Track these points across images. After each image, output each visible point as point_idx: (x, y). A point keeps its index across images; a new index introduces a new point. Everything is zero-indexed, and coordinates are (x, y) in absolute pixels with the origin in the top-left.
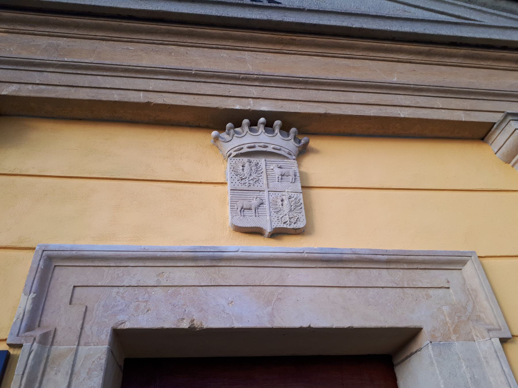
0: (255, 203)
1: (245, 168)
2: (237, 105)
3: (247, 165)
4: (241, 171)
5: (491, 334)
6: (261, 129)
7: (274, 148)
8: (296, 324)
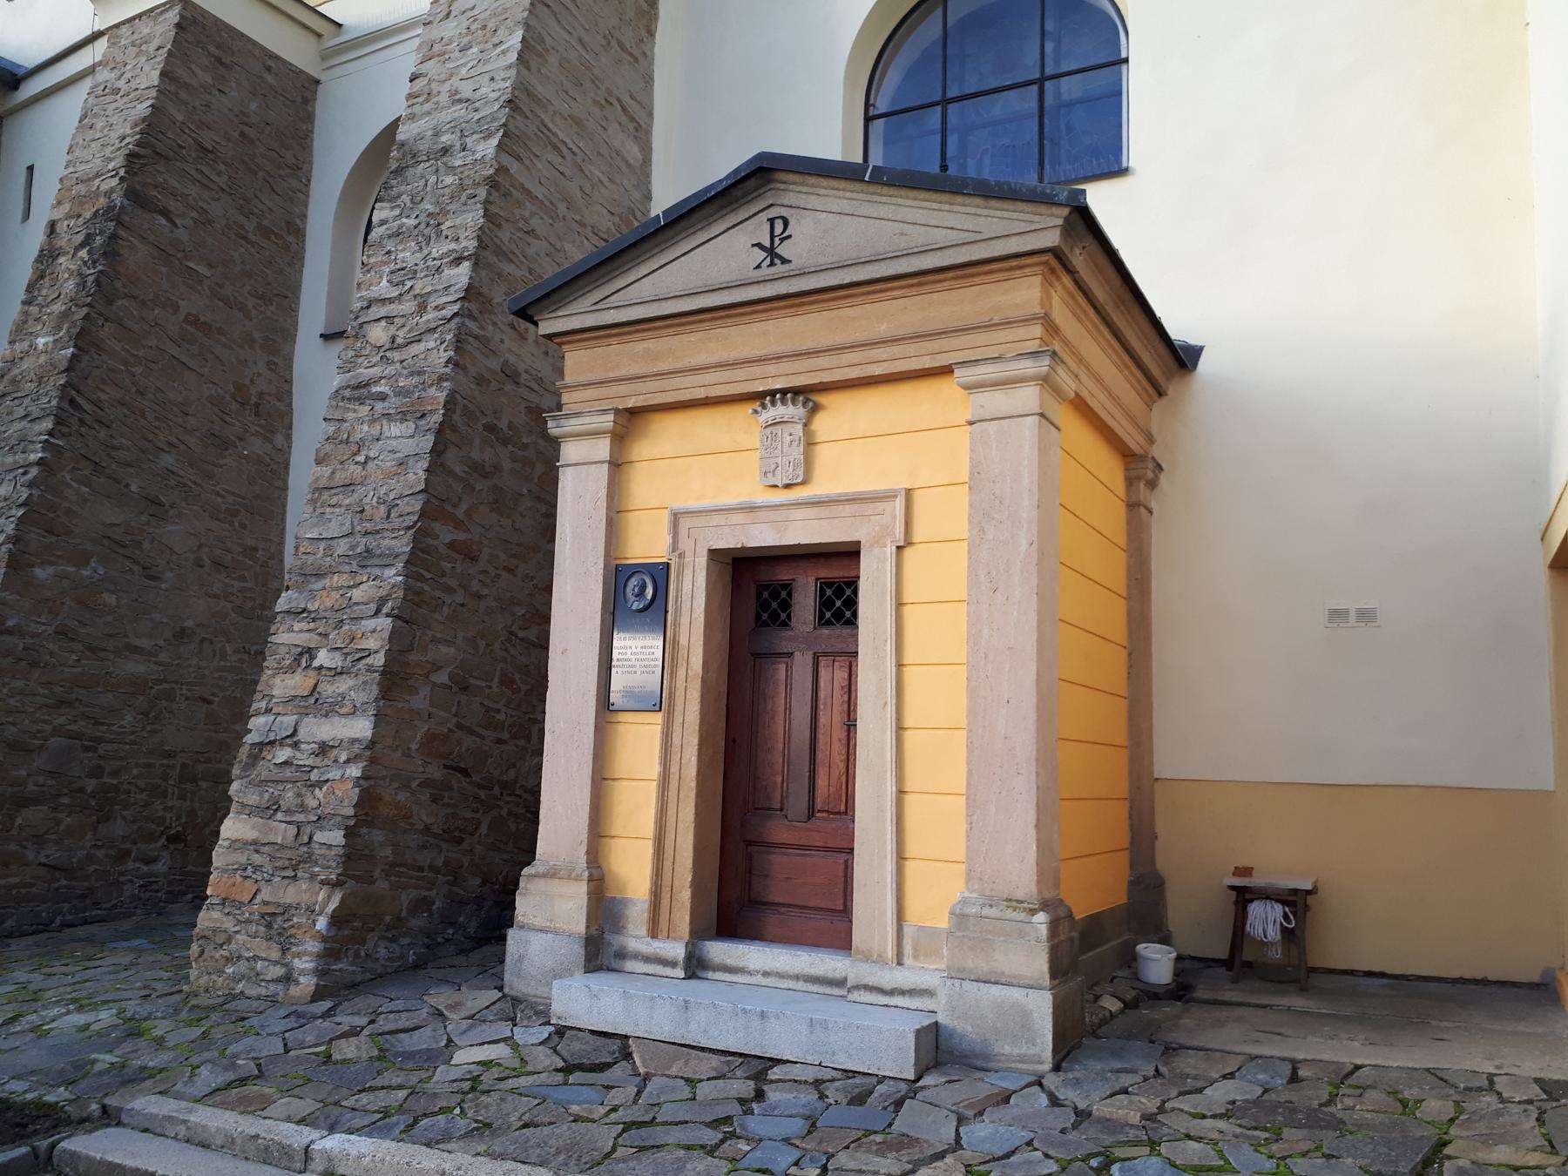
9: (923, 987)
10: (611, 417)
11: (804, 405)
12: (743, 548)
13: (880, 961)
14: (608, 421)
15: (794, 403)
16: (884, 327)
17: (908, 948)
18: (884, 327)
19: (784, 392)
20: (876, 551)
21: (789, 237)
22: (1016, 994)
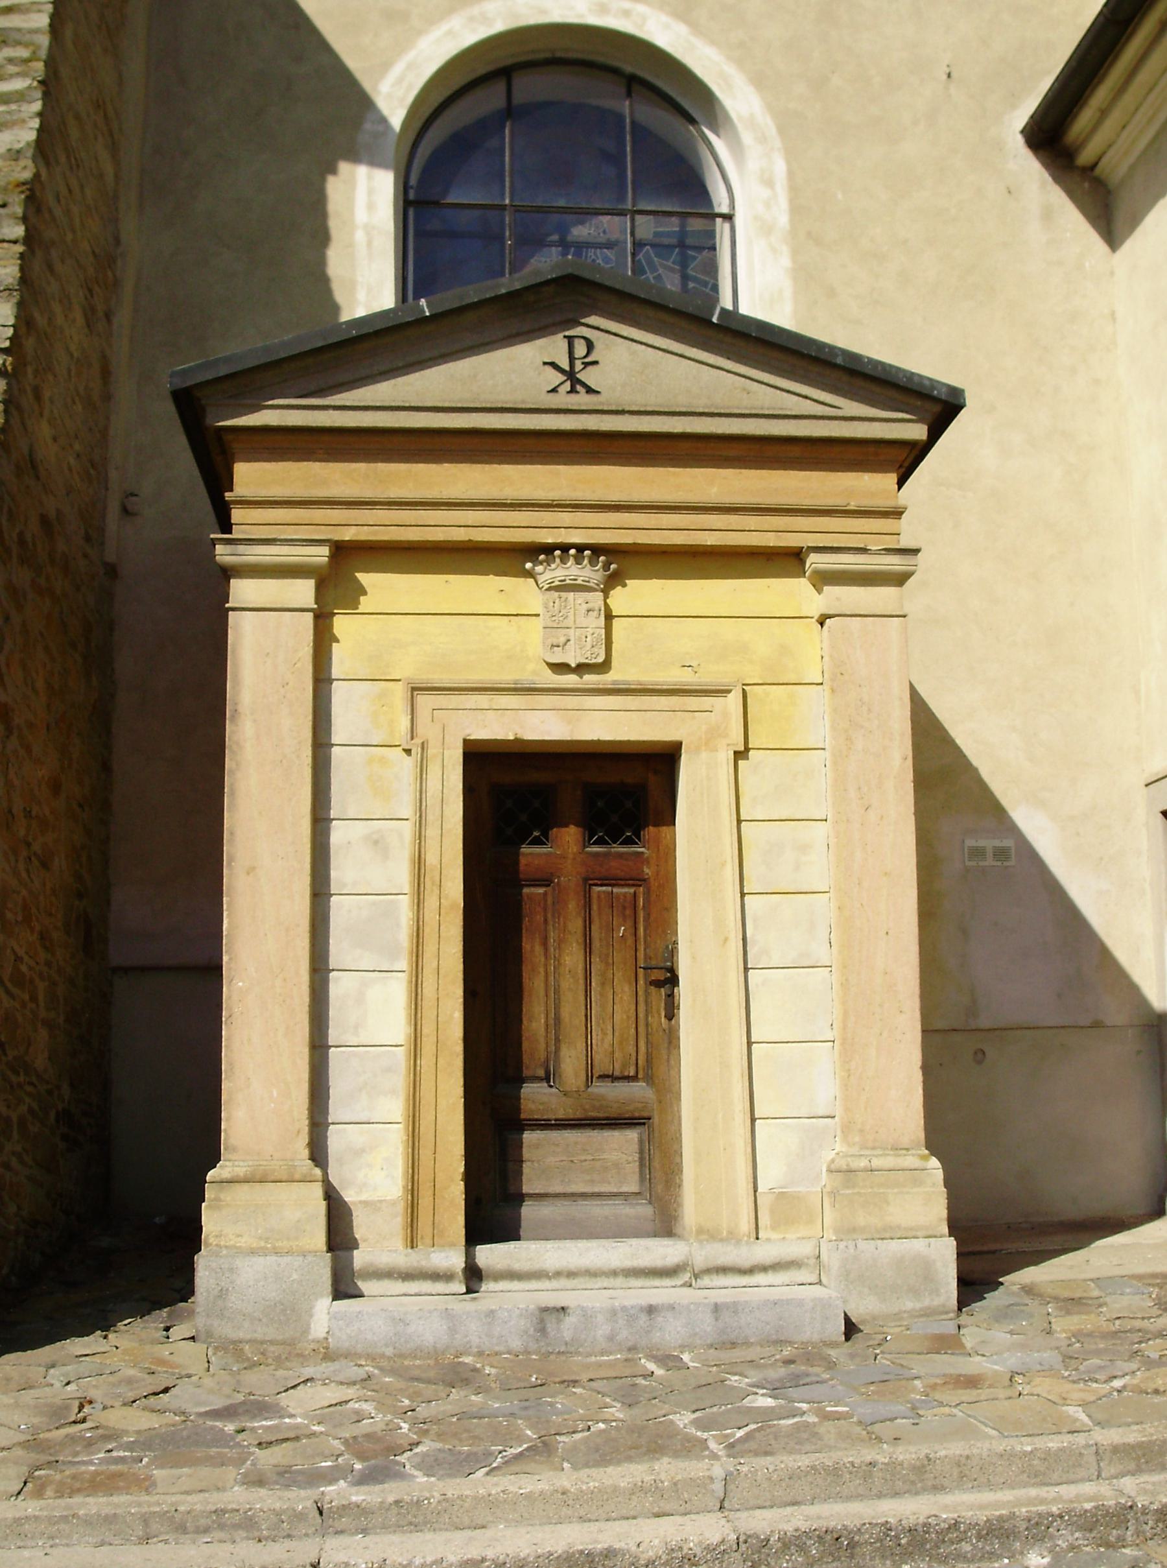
0: (562, 640)
1: (555, 605)
2: (549, 538)
3: (557, 601)
4: (552, 608)
5: (729, 747)
6: (571, 561)
7: (583, 581)
8: (589, 738)
9: (789, 1259)
10: (325, 551)
11: (606, 567)
12: (518, 741)
13: (732, 1237)
14: (320, 555)
15: (593, 563)
16: (715, 490)
17: (764, 1220)
18: (715, 490)
19: (580, 548)
20: (704, 755)
21: (595, 363)
22: (918, 1246)
